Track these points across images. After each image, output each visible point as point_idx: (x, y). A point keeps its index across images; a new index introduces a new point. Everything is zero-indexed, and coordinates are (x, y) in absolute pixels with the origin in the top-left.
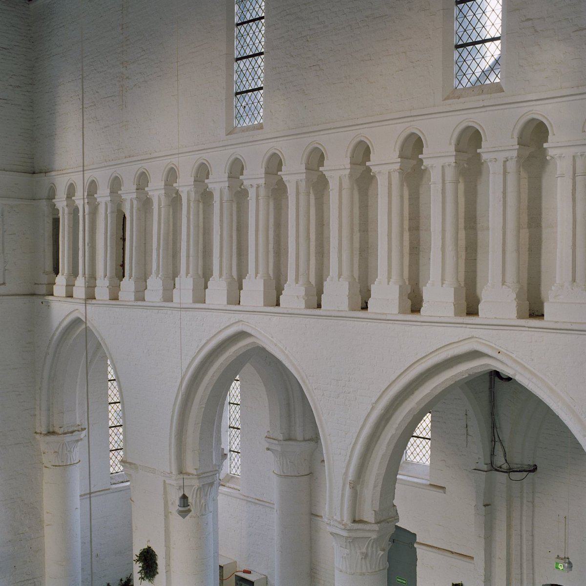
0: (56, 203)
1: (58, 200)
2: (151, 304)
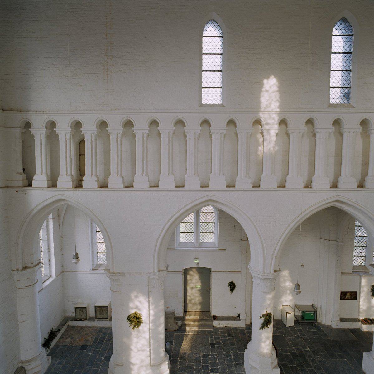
0: (31, 131)
1: (33, 129)
2: (86, 190)
